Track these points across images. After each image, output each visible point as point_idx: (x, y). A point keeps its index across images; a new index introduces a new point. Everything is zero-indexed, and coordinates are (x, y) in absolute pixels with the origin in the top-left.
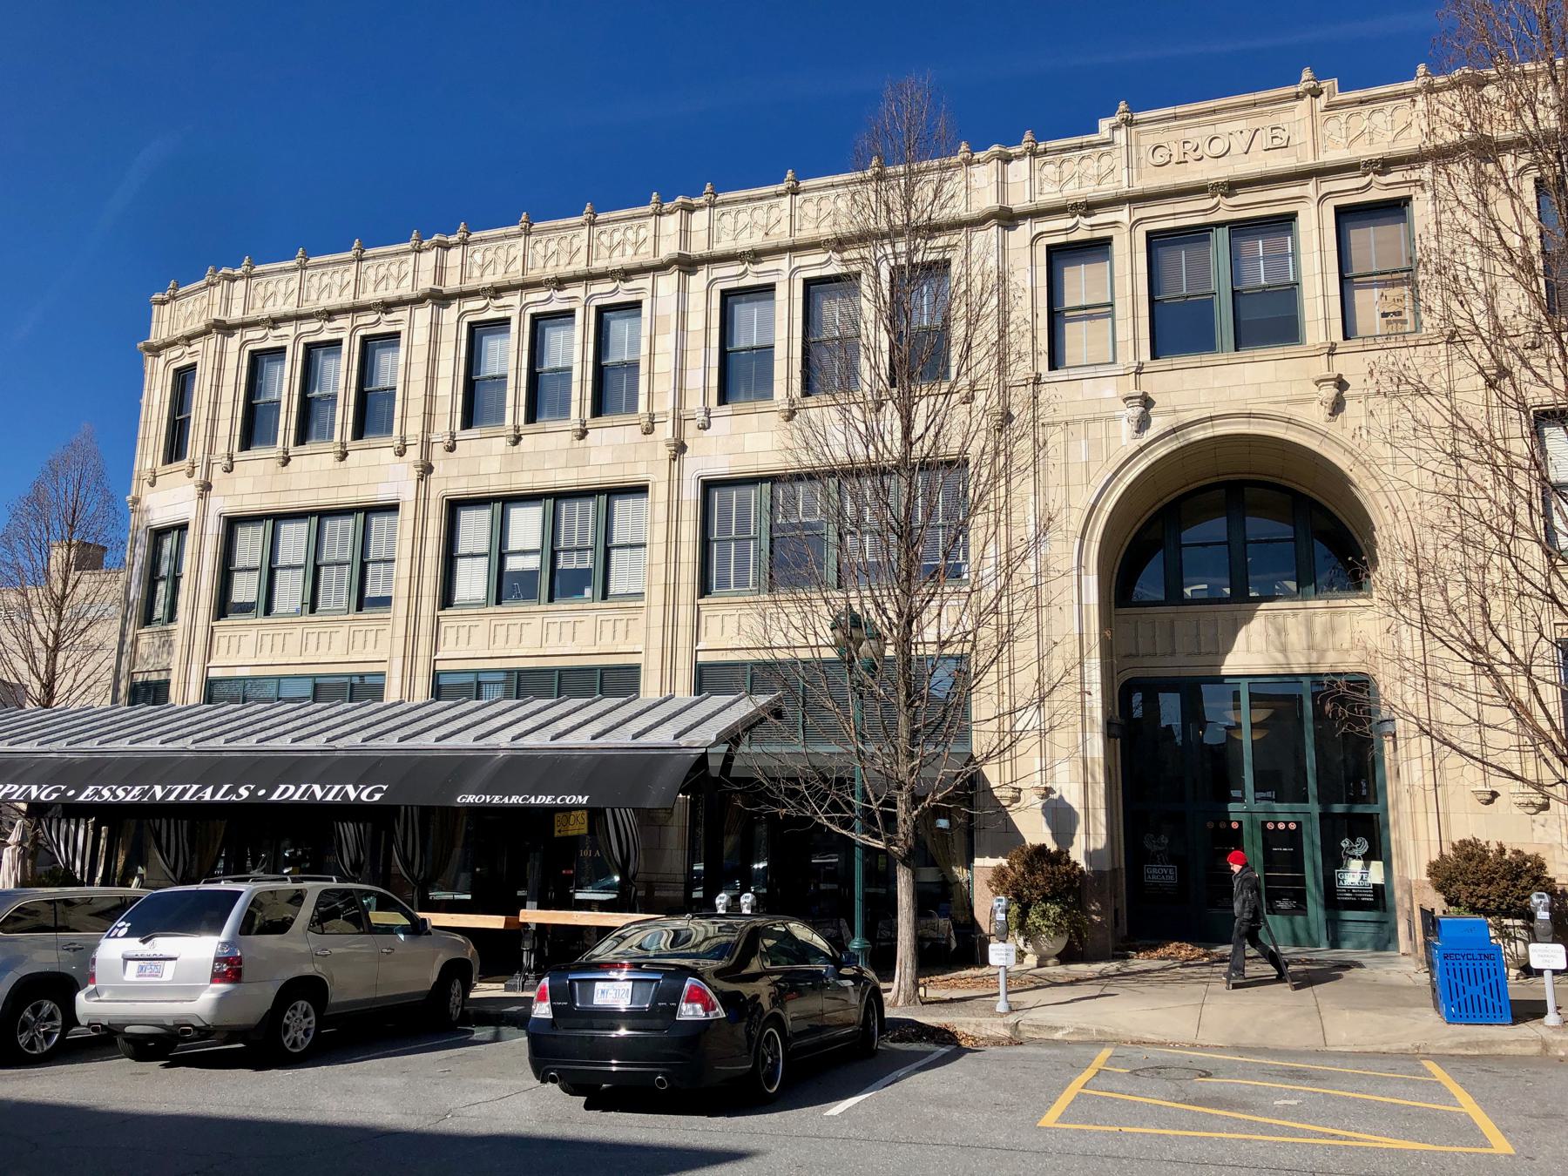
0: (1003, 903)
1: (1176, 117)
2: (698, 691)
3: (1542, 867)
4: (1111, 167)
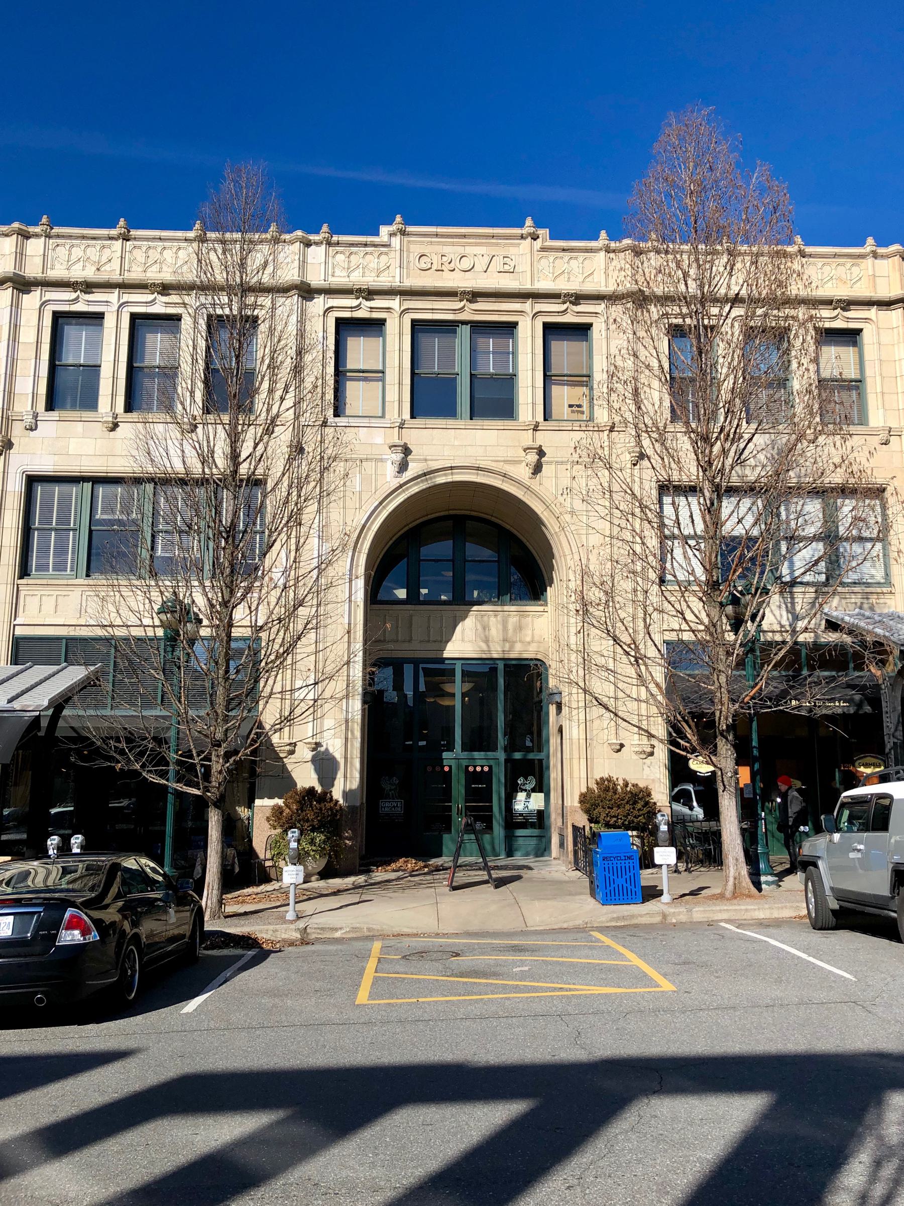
0: (296, 834)
1: (437, 235)
2: (15, 661)
3: (649, 795)
4: (388, 265)
